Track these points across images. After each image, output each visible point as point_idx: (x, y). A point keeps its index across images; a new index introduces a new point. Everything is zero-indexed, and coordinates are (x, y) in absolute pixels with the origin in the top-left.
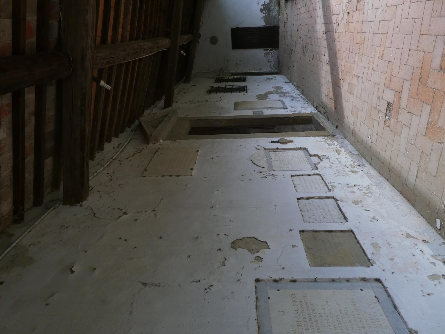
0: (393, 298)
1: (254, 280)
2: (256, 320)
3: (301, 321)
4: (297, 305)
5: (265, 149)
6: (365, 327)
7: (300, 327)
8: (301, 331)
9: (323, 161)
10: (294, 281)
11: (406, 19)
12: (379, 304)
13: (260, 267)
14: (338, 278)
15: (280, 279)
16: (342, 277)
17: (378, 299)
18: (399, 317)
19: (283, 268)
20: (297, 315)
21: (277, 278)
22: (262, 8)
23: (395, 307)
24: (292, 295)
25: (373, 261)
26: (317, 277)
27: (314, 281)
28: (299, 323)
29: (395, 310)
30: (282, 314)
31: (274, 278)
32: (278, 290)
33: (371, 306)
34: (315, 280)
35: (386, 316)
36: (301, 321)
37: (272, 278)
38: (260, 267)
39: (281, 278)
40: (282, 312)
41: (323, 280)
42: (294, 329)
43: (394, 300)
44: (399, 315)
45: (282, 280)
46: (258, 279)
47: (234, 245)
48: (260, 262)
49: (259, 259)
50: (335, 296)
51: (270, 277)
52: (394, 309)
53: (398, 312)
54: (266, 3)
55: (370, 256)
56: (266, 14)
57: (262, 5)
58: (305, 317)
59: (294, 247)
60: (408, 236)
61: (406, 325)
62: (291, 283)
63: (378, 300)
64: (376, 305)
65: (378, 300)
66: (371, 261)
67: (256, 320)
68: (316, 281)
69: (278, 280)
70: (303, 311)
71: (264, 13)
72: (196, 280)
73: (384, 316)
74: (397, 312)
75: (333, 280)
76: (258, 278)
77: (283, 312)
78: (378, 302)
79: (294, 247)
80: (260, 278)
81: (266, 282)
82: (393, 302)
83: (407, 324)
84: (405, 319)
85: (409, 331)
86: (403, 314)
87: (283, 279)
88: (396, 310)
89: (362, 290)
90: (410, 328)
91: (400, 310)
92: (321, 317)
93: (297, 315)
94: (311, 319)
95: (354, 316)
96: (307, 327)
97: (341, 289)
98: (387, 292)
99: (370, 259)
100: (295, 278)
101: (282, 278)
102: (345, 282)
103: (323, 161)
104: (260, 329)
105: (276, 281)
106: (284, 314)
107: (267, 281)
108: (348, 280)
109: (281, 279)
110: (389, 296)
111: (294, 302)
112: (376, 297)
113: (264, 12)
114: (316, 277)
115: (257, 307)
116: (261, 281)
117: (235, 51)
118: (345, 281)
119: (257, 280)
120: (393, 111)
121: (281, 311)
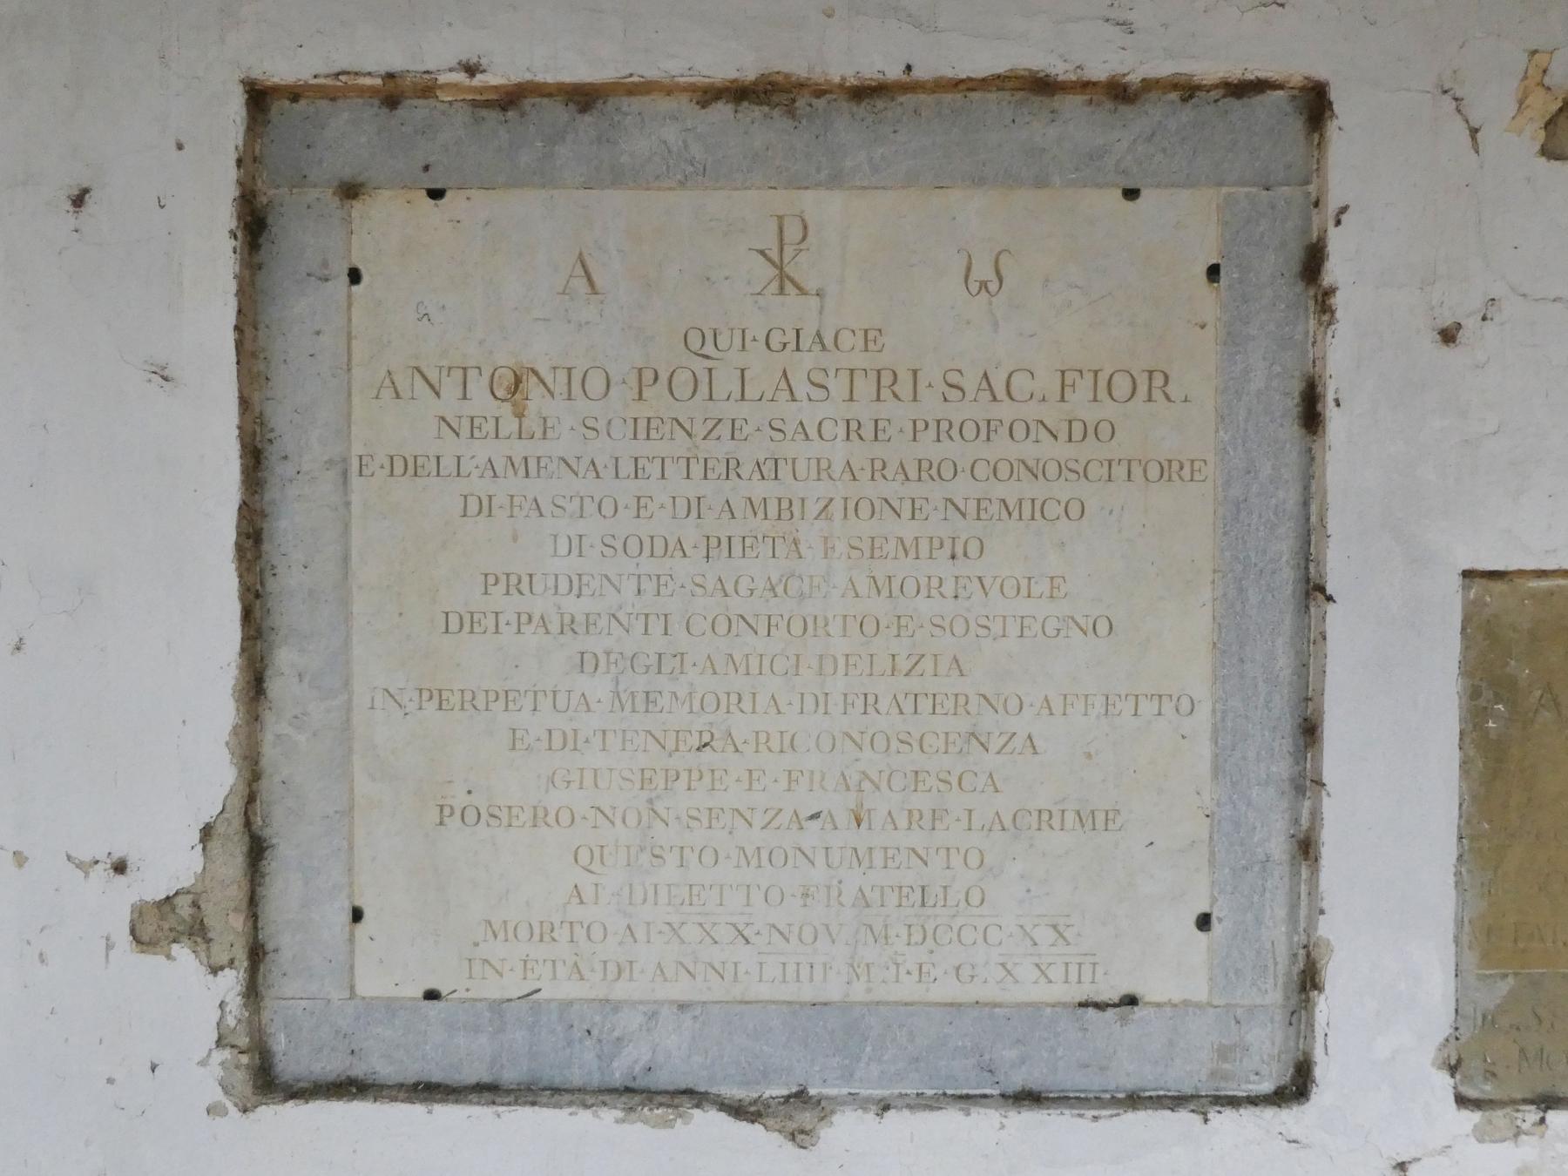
0: (1096, 1118)
1: (1320, 73)
2: (909, 68)
3: (915, 399)
4: (1063, 399)
6: (864, 825)
7: (865, 387)
8: (838, 386)
9: (1395, 1168)
10: (1311, 416)
12: (1067, 999)
13: (1474, 132)
14: (1318, 769)
15: (1330, 292)
16: (1328, 806)
17: (1110, 1012)
18: (949, 1092)
19: (1448, 336)
20: (971, 382)
21: (1335, 271)
23: (1029, 1098)
24: (1158, 380)
25: (1518, 1133)
26: (1330, 599)
27: (1308, 581)
28: (904, 388)
29: (1010, 1091)
30: (983, 271)
31: (1339, 246)
32: (1213, 272)
33: (1044, 935)
34: (1314, 591)
35: (951, 1005)
36: (915, 399)
37: (1338, 223)
38: (1474, 132)
39: (1338, 301)
40: (992, 276)
42: (846, 340)
43: (1081, 1116)
44: (958, 1092)
45: (1324, 311)
46: (1330, 103)
48: (1542, 134)
50: (1148, 708)
51: (1343, 210)
52: (1017, 1080)
53: (985, 1096)
58: (955, 433)
61: (857, 1101)
62: (1297, 387)
63: (1100, 1006)
64: (1056, 973)
65: (1100, 1006)
66: (1531, 1115)
67: (909, 68)
68: (1307, 594)
69: (1319, 282)
70: (1004, 431)
73: (946, 990)
74: (988, 1091)
75: (1310, 731)
76: (1335, 107)
77: (993, 287)
78: (1083, 998)
80: (1332, 128)
81: (1307, 182)
82: (1072, 1107)
83: (865, 1109)
84: (906, 1112)
85: (828, 1098)
86: (950, 1119)
87: (1326, 318)
88: (1003, 1096)
89: (1204, 922)
90: (833, 1112)
91: (986, 1120)
92: (947, 551)
93: (971, 382)
94: (934, 472)
95: (955, 783)
96: (867, 431)
97: (1217, 771)
98: (1177, 1101)
99: (1548, 1108)
100: (1335, 421)
101: (1333, 312)
102: (1296, 821)
103: (1395, 1168)
104: (845, 105)
105: (1313, 261)
106: (974, 287)
107: (1312, 188)
108: (1306, 848)
109: (1324, 304)
110: (1134, 1100)
111: (1089, 377)
112: (1131, 1001)
114: (1329, 591)
115: (1042, 86)
116: (1316, 136)
118: (1305, 822)
120: (645, 74)
121: (1004, 272)
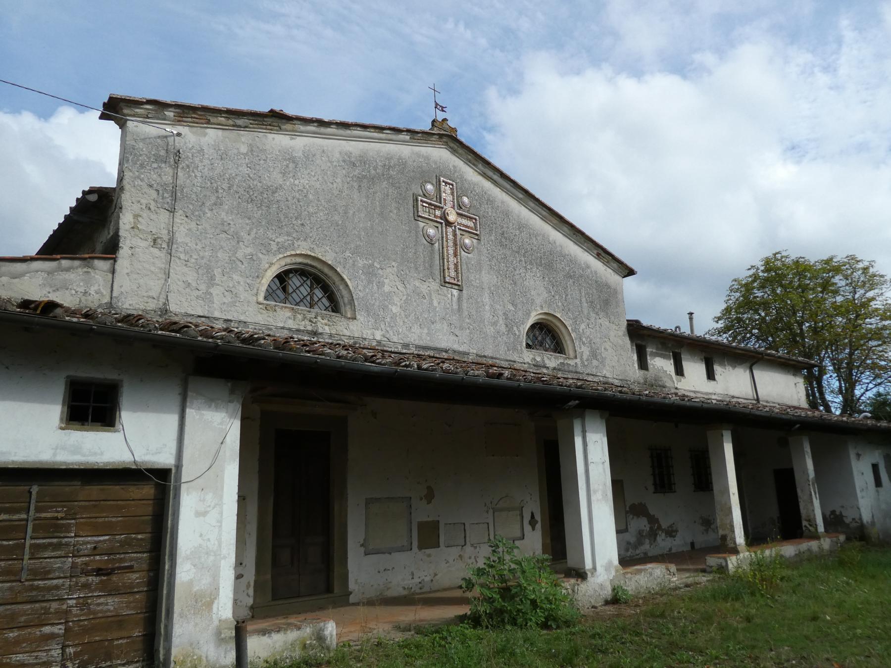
5: (522, 507)
10: (411, 514)
11: (465, 537)
22: (838, 513)
41: (411, 526)
47: (429, 488)
49: (421, 499)
54: (845, 519)
55: (423, 550)
56: (829, 519)
57: (841, 512)
59: (429, 516)
60: (436, 575)
71: (830, 516)
72: (264, 649)
79: (429, 516)
108: (411, 537)
113: (832, 516)
117: (871, 465)
119: (411, 498)
